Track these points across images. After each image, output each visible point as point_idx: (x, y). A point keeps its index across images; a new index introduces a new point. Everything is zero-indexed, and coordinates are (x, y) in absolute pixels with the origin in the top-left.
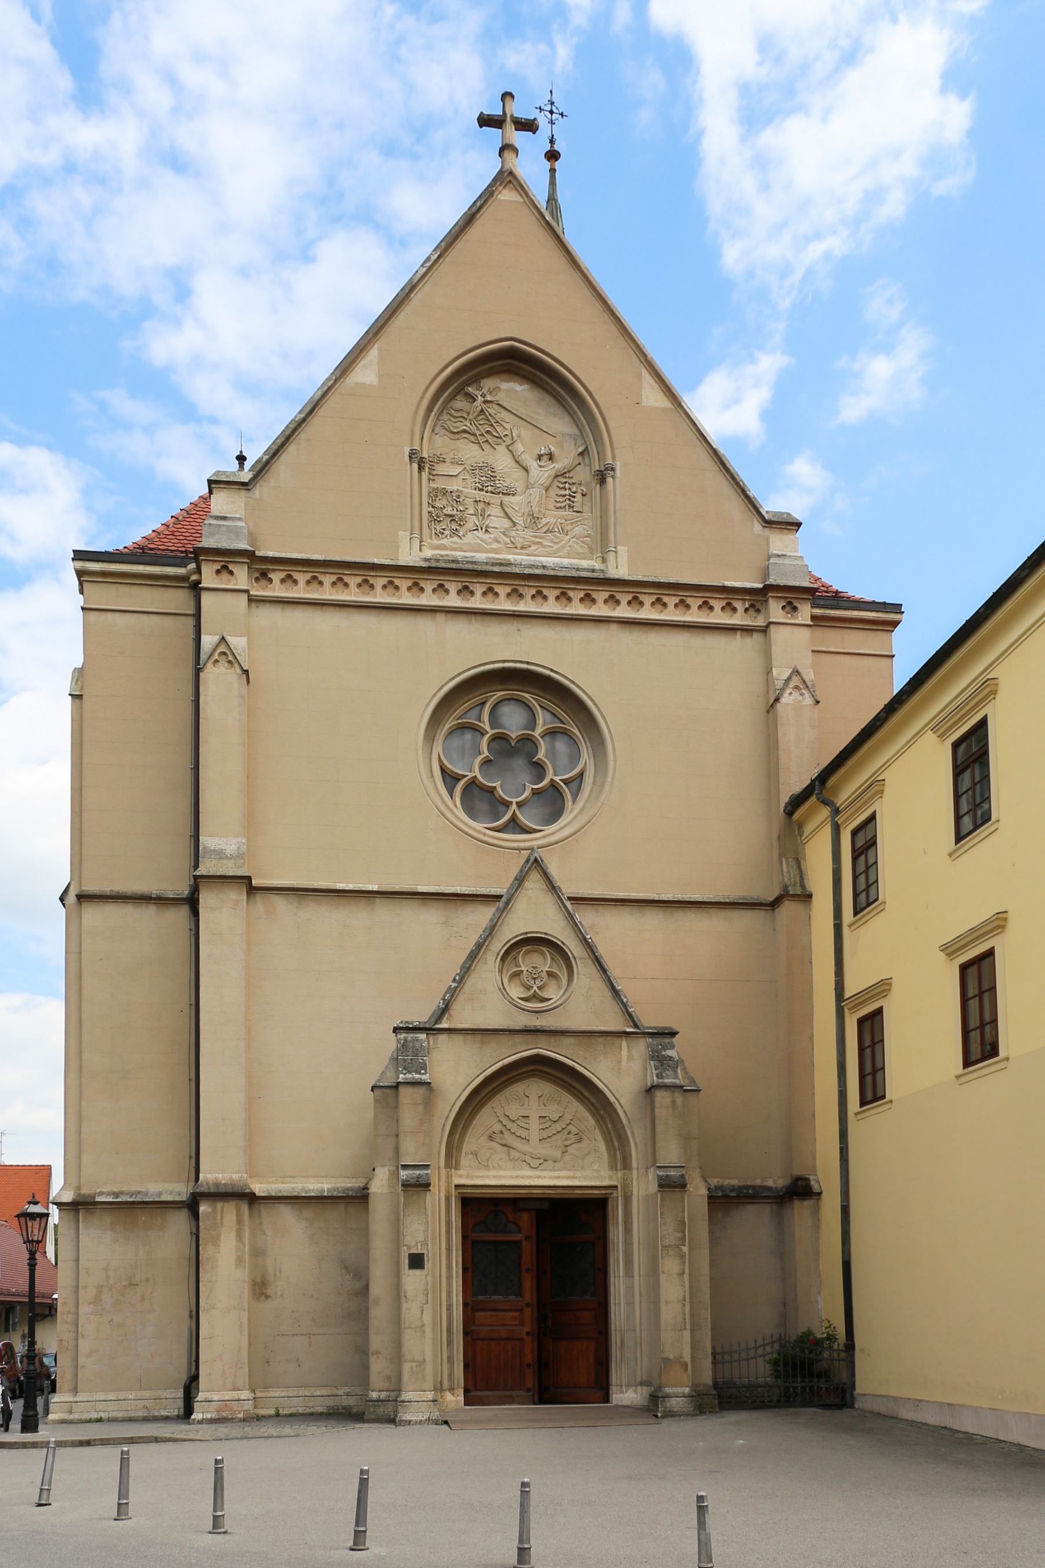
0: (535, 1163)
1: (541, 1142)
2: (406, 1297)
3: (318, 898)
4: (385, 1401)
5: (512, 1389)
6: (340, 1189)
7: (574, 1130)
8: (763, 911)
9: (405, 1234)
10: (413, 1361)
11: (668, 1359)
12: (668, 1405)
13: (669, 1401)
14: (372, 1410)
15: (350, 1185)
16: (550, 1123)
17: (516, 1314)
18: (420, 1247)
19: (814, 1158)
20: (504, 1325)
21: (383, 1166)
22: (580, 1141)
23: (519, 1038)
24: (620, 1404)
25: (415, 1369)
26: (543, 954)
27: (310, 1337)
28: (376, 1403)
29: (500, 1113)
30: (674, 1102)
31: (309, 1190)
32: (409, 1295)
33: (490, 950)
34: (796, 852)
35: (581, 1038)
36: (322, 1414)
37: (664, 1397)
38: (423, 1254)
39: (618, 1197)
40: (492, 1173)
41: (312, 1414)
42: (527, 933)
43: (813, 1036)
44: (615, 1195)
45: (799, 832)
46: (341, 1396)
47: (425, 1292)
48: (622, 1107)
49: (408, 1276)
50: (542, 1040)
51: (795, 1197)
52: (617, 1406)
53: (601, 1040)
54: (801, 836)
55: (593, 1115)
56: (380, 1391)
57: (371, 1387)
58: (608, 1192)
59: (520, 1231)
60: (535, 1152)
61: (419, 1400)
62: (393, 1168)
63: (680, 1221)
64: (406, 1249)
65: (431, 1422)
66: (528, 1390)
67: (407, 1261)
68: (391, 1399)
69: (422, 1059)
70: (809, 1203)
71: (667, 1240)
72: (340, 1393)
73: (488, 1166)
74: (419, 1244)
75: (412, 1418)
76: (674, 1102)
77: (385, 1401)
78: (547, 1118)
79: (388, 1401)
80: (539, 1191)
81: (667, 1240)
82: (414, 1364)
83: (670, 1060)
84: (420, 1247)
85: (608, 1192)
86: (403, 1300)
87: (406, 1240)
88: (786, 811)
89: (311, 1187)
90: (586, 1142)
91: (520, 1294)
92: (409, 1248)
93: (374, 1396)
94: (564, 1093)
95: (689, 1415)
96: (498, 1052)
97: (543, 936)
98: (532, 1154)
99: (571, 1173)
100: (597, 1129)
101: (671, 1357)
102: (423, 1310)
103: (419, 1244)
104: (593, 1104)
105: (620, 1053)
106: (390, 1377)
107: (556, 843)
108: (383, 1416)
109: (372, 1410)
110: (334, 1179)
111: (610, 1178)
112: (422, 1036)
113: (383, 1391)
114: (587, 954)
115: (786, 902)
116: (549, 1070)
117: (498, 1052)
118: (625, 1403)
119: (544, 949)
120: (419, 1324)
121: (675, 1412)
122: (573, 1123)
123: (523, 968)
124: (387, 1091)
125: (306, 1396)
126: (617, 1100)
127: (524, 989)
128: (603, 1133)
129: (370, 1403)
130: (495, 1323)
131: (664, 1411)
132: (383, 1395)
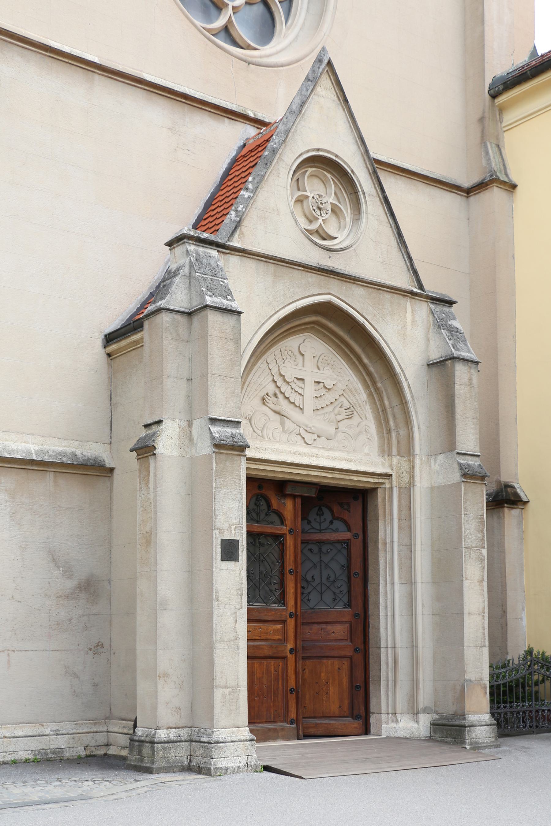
0: (309, 438)
1: (315, 411)
2: (217, 598)
3: (27, 52)
4: (176, 742)
5: (275, 722)
6: (50, 453)
7: (346, 404)
8: (459, 197)
9: (217, 513)
10: (226, 687)
11: (471, 681)
12: (474, 736)
13: (475, 732)
14: (161, 754)
15: (61, 449)
16: (324, 391)
17: (279, 626)
18: (233, 532)
19: (516, 465)
20: (266, 640)
21: (173, 419)
22: (350, 417)
23: (312, 278)
24: (392, 736)
25: (227, 696)
26: (324, 182)
27: (8, 655)
28: (166, 745)
29: (275, 371)
30: (471, 379)
31: (13, 450)
32: (221, 596)
33: (283, 161)
34: (497, 138)
35: (370, 289)
36: (27, 761)
37: (469, 726)
38: (238, 541)
39: (391, 488)
40: (267, 445)
41: (14, 762)
42: (318, 150)
43: (515, 335)
44: (387, 485)
45: (500, 119)
46: (49, 735)
47: (239, 593)
48: (406, 380)
49: (220, 570)
50: (334, 285)
51: (506, 505)
52: (388, 737)
53: (387, 296)
54: (501, 123)
55: (367, 387)
56: (168, 728)
57: (215, 726)
58: (381, 481)
59: (283, 523)
60: (311, 425)
61: (234, 740)
62: (184, 424)
63: (479, 518)
64: (218, 533)
65: (250, 768)
66: (291, 723)
67: (219, 550)
68: (183, 738)
69: (223, 282)
70: (515, 512)
71: (469, 541)
72: (47, 732)
73: (262, 436)
74: (233, 527)
75: (229, 765)
76: (471, 379)
77: (176, 742)
78: (322, 385)
79: (180, 741)
80: (316, 474)
81: (469, 541)
82: (227, 691)
83: (457, 332)
84: (233, 532)
85: (381, 481)
86: (215, 603)
87: (217, 520)
88: (492, 91)
89: (14, 446)
90: (356, 419)
91: (282, 599)
92: (221, 532)
93: (163, 736)
94: (338, 356)
95: (491, 746)
96: (291, 290)
97: (334, 158)
98: (307, 426)
99: (344, 455)
100: (368, 404)
101: (473, 679)
102: (236, 616)
103: (233, 527)
104: (369, 374)
105: (405, 316)
106: (180, 709)
107: (282, 66)
108: (174, 762)
109: (161, 754)
110: (41, 439)
111: (383, 464)
112: (214, 253)
113: (171, 728)
114: (375, 191)
115: (495, 189)
116: (331, 325)
117: (291, 290)
118: (400, 734)
119: (329, 175)
120: (232, 636)
121: (481, 743)
122: (345, 395)
123: (308, 194)
124: (178, 317)
125: (5, 737)
126: (402, 371)
127: (306, 220)
128: (375, 410)
129: (159, 745)
130: (257, 638)
131: (471, 744)
132: (173, 734)
